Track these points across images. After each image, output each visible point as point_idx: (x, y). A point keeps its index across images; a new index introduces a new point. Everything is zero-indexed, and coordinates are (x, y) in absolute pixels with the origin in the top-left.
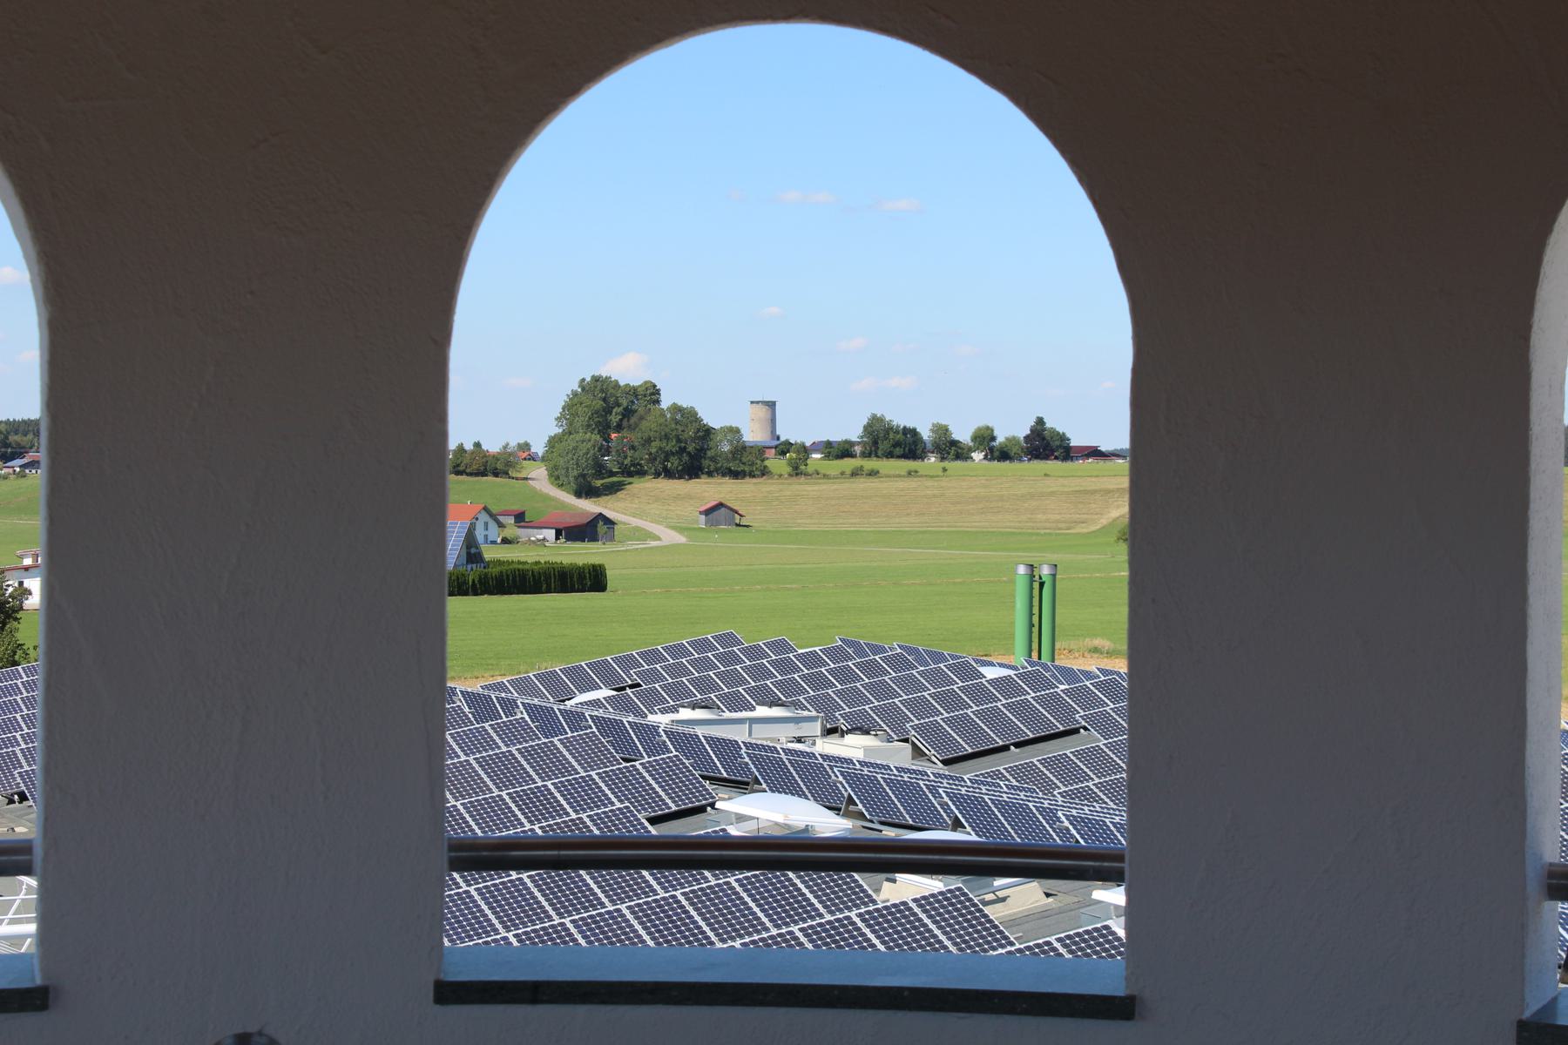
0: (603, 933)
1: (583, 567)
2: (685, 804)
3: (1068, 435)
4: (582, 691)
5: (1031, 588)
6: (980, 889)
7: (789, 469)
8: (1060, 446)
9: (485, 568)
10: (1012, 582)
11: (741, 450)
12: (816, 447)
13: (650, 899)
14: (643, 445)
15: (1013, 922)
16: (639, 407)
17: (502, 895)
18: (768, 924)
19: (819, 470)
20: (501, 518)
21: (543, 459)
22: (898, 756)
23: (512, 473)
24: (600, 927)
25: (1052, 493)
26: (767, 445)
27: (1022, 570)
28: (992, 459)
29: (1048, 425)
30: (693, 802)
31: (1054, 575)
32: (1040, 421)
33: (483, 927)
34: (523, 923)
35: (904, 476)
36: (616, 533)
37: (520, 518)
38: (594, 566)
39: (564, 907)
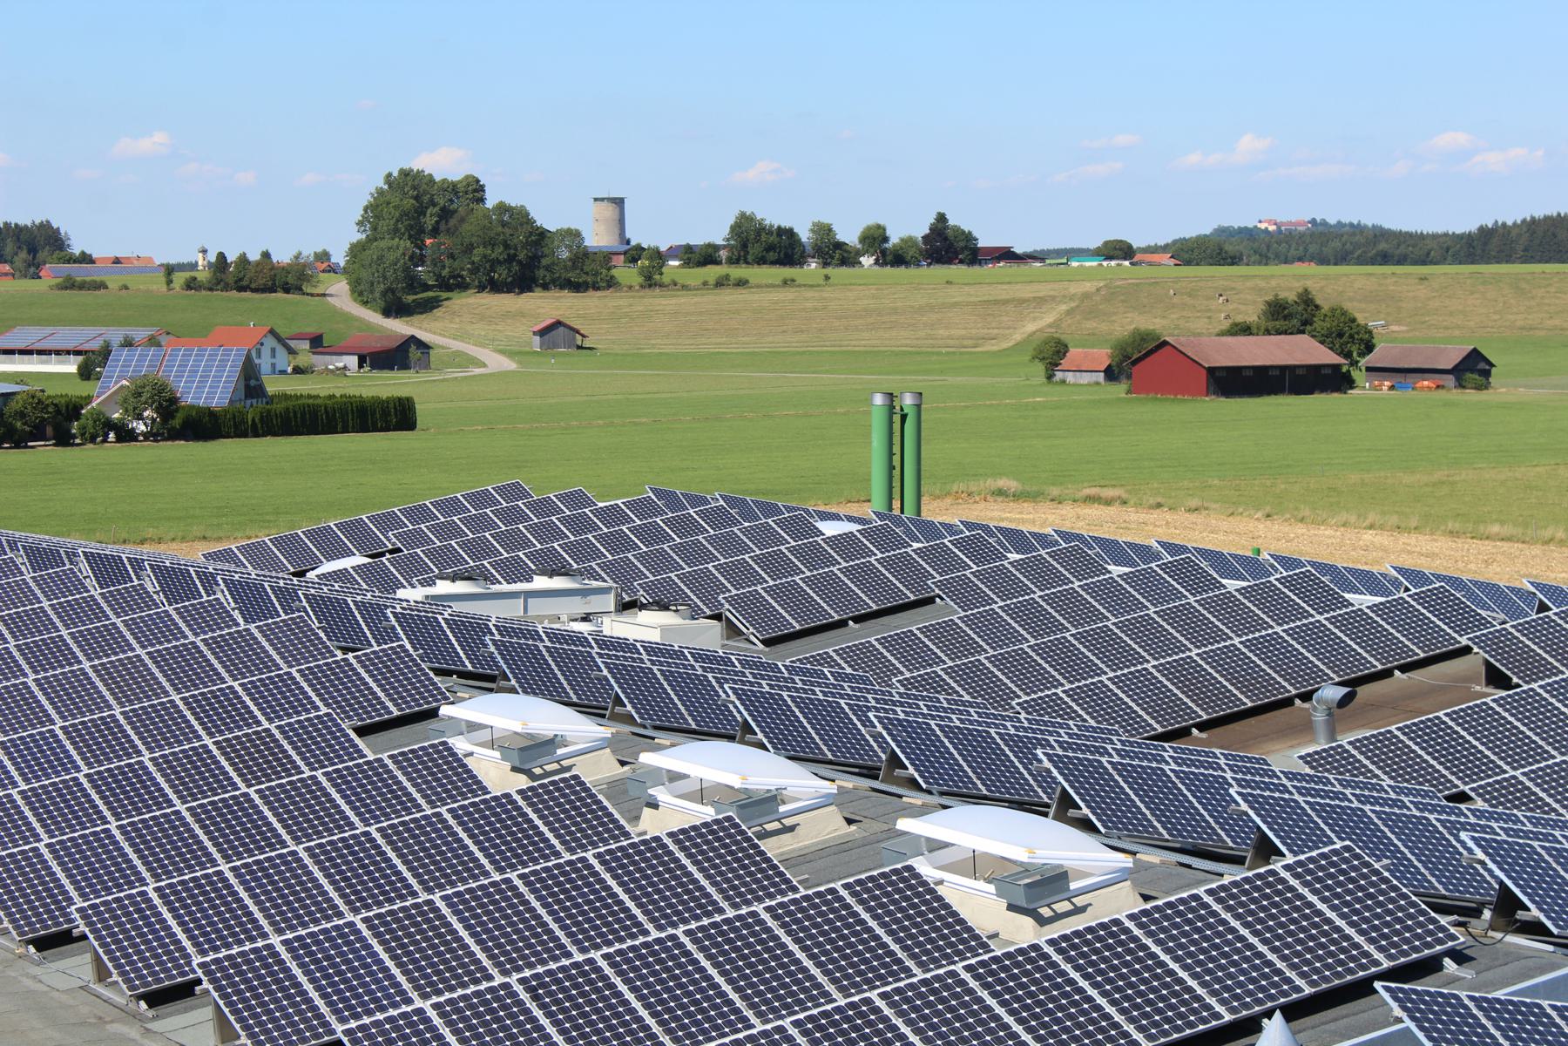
0: (272, 883)
1: (388, 400)
2: (411, 707)
3: (975, 234)
4: (330, 558)
5: (891, 423)
6: (760, 816)
7: (640, 280)
8: (966, 247)
9: (267, 403)
10: (868, 413)
11: (583, 256)
12: (674, 252)
13: (324, 841)
14: (465, 252)
15: (798, 860)
16: (460, 206)
17: (152, 833)
18: (489, 867)
19: (677, 280)
20: (292, 343)
21: (345, 271)
22: (708, 636)
23: (307, 288)
24: (268, 876)
25: (955, 304)
26: (615, 250)
27: (879, 400)
28: (885, 264)
29: (952, 222)
30: (420, 705)
31: (918, 406)
32: (941, 218)
33: (125, 876)
34: (328, 830)
35: (778, 286)
36: (432, 359)
37: (317, 342)
38: (400, 399)
39: (370, 811)
